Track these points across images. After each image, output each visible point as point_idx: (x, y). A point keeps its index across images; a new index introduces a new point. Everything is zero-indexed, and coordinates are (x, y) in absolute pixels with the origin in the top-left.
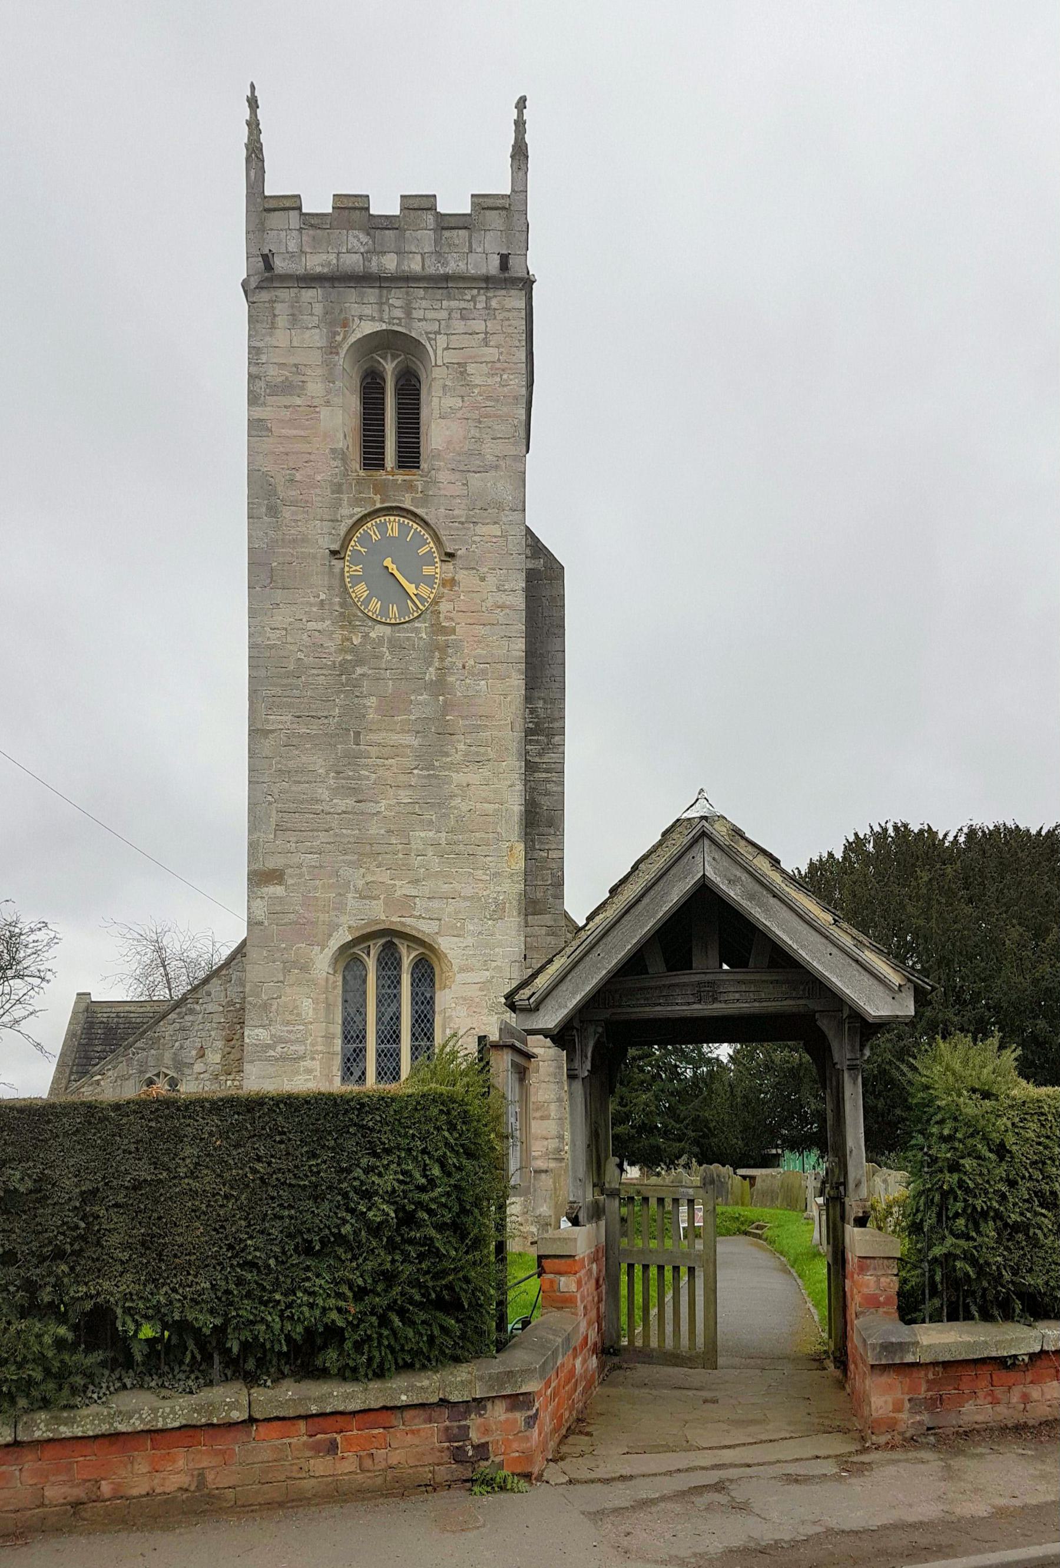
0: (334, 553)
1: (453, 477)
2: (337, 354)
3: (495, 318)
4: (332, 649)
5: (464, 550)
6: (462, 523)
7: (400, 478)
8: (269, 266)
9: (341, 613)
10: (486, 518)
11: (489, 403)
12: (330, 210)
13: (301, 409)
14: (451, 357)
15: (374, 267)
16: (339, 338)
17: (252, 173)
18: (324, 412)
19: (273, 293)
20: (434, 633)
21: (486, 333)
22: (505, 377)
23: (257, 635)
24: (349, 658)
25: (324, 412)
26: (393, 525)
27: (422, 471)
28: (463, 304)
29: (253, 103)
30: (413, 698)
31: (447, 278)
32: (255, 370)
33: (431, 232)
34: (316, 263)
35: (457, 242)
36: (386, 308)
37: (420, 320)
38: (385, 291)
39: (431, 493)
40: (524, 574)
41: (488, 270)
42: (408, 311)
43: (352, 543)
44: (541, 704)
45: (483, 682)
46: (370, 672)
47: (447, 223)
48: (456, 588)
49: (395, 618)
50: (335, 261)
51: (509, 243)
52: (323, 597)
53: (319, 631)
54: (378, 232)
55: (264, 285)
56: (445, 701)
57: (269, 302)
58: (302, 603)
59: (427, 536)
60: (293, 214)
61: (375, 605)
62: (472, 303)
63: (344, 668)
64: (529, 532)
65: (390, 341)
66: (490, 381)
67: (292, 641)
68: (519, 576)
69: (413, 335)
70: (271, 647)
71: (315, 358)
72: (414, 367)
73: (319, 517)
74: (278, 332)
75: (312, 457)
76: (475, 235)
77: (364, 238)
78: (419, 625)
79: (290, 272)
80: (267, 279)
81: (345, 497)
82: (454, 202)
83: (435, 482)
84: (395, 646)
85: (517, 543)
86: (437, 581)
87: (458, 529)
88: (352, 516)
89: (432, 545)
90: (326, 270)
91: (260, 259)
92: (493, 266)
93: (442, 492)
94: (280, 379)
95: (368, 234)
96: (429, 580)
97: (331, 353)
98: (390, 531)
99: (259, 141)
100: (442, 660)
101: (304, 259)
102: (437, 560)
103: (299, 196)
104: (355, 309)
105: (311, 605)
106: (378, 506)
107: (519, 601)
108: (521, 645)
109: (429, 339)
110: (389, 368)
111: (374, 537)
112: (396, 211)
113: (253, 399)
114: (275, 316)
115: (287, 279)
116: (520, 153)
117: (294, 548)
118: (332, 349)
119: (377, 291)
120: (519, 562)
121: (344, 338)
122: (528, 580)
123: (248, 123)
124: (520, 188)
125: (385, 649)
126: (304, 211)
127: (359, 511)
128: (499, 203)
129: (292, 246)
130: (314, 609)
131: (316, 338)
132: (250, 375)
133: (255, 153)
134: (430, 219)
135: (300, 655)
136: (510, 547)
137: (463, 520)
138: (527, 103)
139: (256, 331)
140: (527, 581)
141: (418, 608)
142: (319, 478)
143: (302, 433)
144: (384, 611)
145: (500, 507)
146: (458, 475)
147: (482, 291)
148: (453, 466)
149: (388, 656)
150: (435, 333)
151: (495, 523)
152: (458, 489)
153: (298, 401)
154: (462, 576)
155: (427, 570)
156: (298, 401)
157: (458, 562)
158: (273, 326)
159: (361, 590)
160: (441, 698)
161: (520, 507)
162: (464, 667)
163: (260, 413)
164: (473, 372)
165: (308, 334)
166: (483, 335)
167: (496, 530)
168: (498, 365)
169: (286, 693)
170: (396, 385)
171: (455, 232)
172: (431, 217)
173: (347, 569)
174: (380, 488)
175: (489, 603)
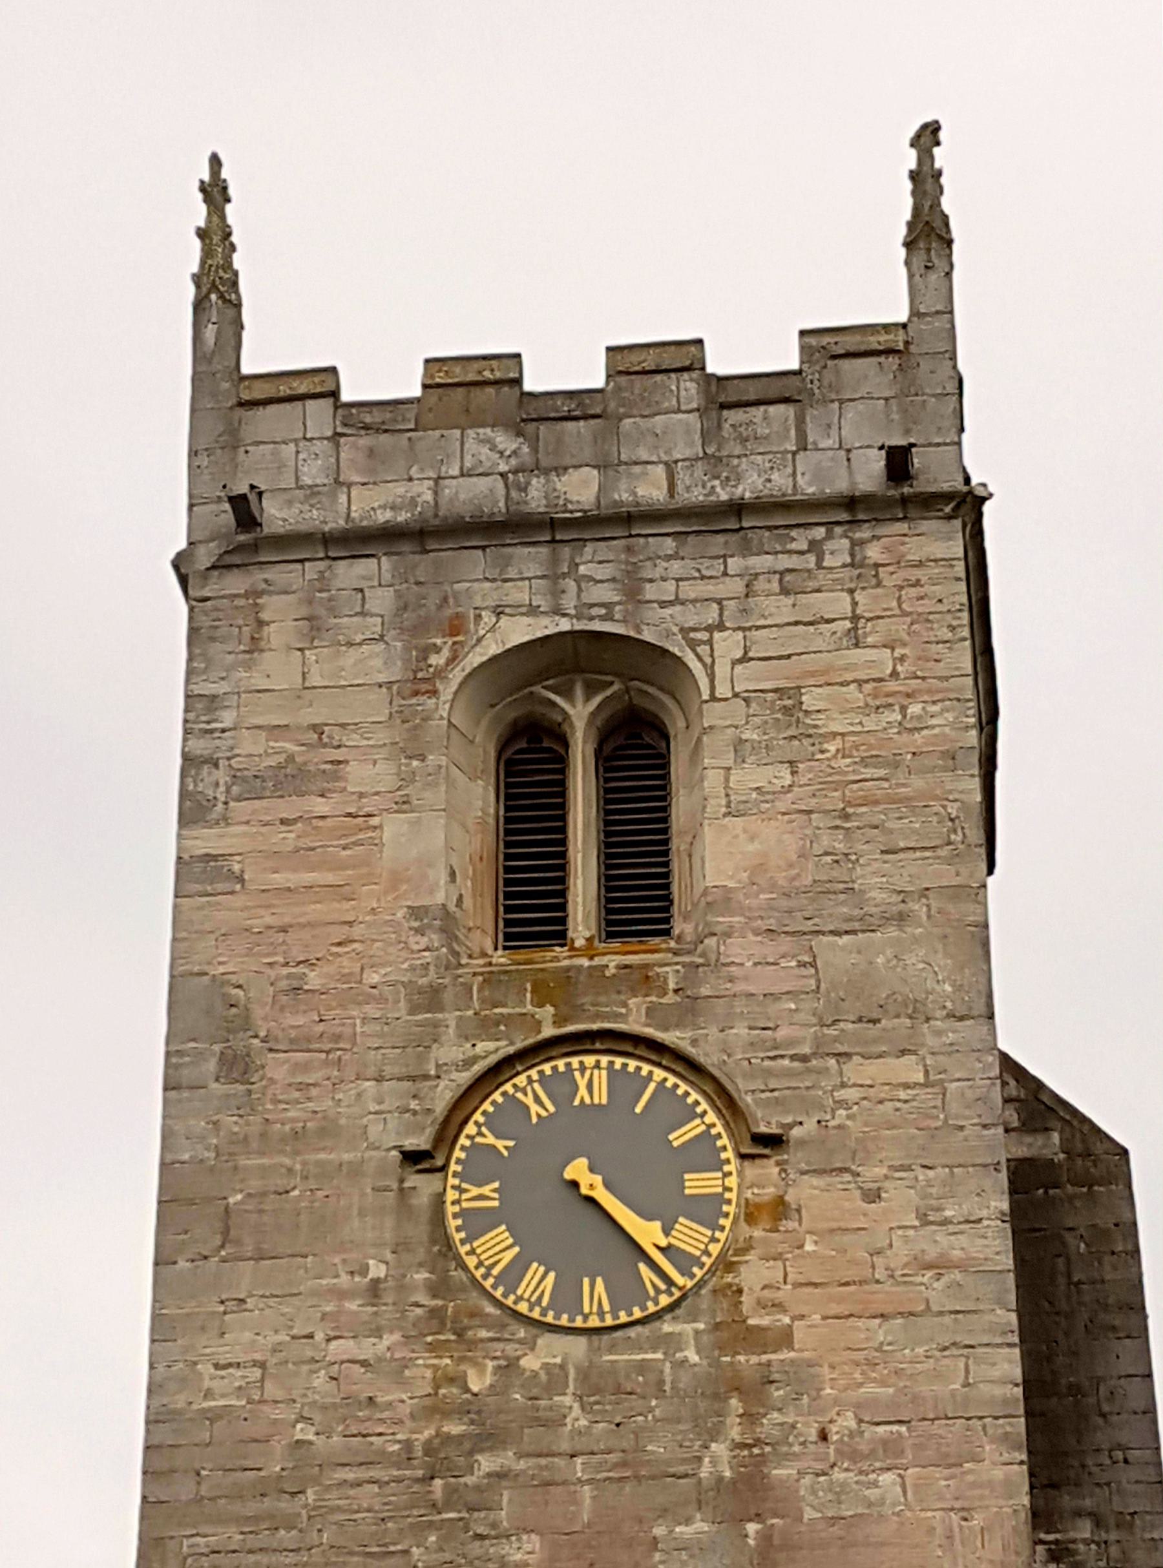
0: (412, 1158)
1: (770, 949)
2: (434, 693)
3: (879, 584)
4: (404, 1410)
5: (810, 1125)
6: (804, 1059)
7: (612, 962)
8: (244, 511)
9: (434, 1312)
10: (875, 1041)
11: (869, 772)
12: (417, 392)
13: (329, 822)
14: (748, 678)
15: (536, 497)
16: (436, 660)
17: (210, 332)
18: (393, 827)
19: (258, 577)
20: (722, 1348)
21: (855, 618)
22: (915, 709)
23: (173, 1386)
24: (455, 1428)
25: (393, 827)
26: (592, 1078)
27: (679, 939)
28: (785, 562)
29: (215, 193)
30: (659, 1531)
31: (738, 508)
32: (199, 746)
33: (693, 418)
34: (372, 504)
35: (762, 431)
36: (571, 585)
37: (663, 604)
38: (566, 551)
39: (705, 991)
40: (1003, 1176)
41: (853, 484)
42: (632, 587)
43: (471, 1129)
44: (1084, 1530)
45: (887, 1478)
46: (522, 1464)
47: (729, 396)
48: (791, 1225)
49: (601, 1314)
50: (428, 496)
51: (909, 422)
52: (377, 1270)
53: (364, 1363)
54: (543, 428)
55: (228, 560)
56: (766, 1538)
57: (246, 595)
58: (315, 1293)
59: (694, 1096)
60: (319, 410)
61: (538, 1284)
62: (812, 559)
63: (439, 1460)
64: (1009, 1065)
65: (575, 656)
66: (870, 724)
67: (280, 1395)
68: (987, 1183)
69: (648, 636)
70: (212, 1416)
71: (377, 707)
72: (652, 707)
73: (371, 1071)
74: (267, 660)
75: (357, 931)
76: (810, 413)
77: (506, 441)
78: (677, 1328)
79: (303, 528)
80: (240, 548)
81: (450, 1018)
82: (752, 343)
83: (719, 965)
84: (596, 1386)
85: (976, 1096)
86: (730, 1209)
87: (789, 1073)
88: (469, 1063)
89: (711, 1117)
90: (402, 517)
91: (227, 506)
92: (869, 472)
93: (741, 987)
94: (272, 761)
95: (519, 433)
96: (707, 1210)
97: (416, 693)
98: (583, 1091)
99: (228, 265)
100: (750, 1418)
101: (343, 498)
102: (729, 1154)
103: (333, 371)
104: (485, 594)
105: (342, 1295)
106: (548, 1031)
107: (995, 1248)
108: (1008, 1365)
109: (693, 645)
110: (579, 714)
111: (535, 1109)
112: (597, 380)
113: (193, 810)
114: (261, 623)
115: (293, 543)
116: (929, 235)
117: (297, 1153)
118: (421, 683)
119: (544, 550)
120: (987, 1143)
121: (453, 659)
122: (1016, 1188)
123: (202, 234)
124: (933, 308)
125: (567, 1400)
126: (346, 396)
127: (491, 1050)
128: (874, 342)
129: (313, 473)
130: (352, 1306)
131: (378, 664)
132: (187, 758)
133: (217, 291)
134: (689, 388)
135: (302, 1432)
136: (954, 1107)
137: (806, 1050)
138: (942, 135)
139: (209, 661)
140: (1013, 1191)
141: (670, 1282)
142: (375, 978)
143: (330, 878)
144: (567, 1296)
145: (918, 1012)
146: (786, 944)
147: (838, 530)
148: (772, 923)
149: (577, 1418)
150: (709, 629)
151: (903, 1052)
152: (787, 976)
153: (320, 806)
154: (806, 1191)
155: (697, 1183)
156: (320, 806)
157: (795, 1157)
158: (255, 646)
159: (496, 1247)
160: (752, 1528)
161: (980, 1008)
162: (824, 1436)
163: (206, 841)
164: (820, 705)
165: (351, 657)
166: (848, 624)
167: (910, 1070)
168: (892, 686)
169: (264, 1539)
170: (598, 753)
171: (758, 413)
172: (692, 386)
173: (451, 1195)
174: (555, 990)
175: (900, 1254)
